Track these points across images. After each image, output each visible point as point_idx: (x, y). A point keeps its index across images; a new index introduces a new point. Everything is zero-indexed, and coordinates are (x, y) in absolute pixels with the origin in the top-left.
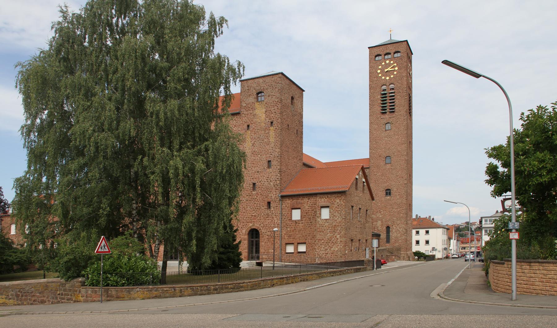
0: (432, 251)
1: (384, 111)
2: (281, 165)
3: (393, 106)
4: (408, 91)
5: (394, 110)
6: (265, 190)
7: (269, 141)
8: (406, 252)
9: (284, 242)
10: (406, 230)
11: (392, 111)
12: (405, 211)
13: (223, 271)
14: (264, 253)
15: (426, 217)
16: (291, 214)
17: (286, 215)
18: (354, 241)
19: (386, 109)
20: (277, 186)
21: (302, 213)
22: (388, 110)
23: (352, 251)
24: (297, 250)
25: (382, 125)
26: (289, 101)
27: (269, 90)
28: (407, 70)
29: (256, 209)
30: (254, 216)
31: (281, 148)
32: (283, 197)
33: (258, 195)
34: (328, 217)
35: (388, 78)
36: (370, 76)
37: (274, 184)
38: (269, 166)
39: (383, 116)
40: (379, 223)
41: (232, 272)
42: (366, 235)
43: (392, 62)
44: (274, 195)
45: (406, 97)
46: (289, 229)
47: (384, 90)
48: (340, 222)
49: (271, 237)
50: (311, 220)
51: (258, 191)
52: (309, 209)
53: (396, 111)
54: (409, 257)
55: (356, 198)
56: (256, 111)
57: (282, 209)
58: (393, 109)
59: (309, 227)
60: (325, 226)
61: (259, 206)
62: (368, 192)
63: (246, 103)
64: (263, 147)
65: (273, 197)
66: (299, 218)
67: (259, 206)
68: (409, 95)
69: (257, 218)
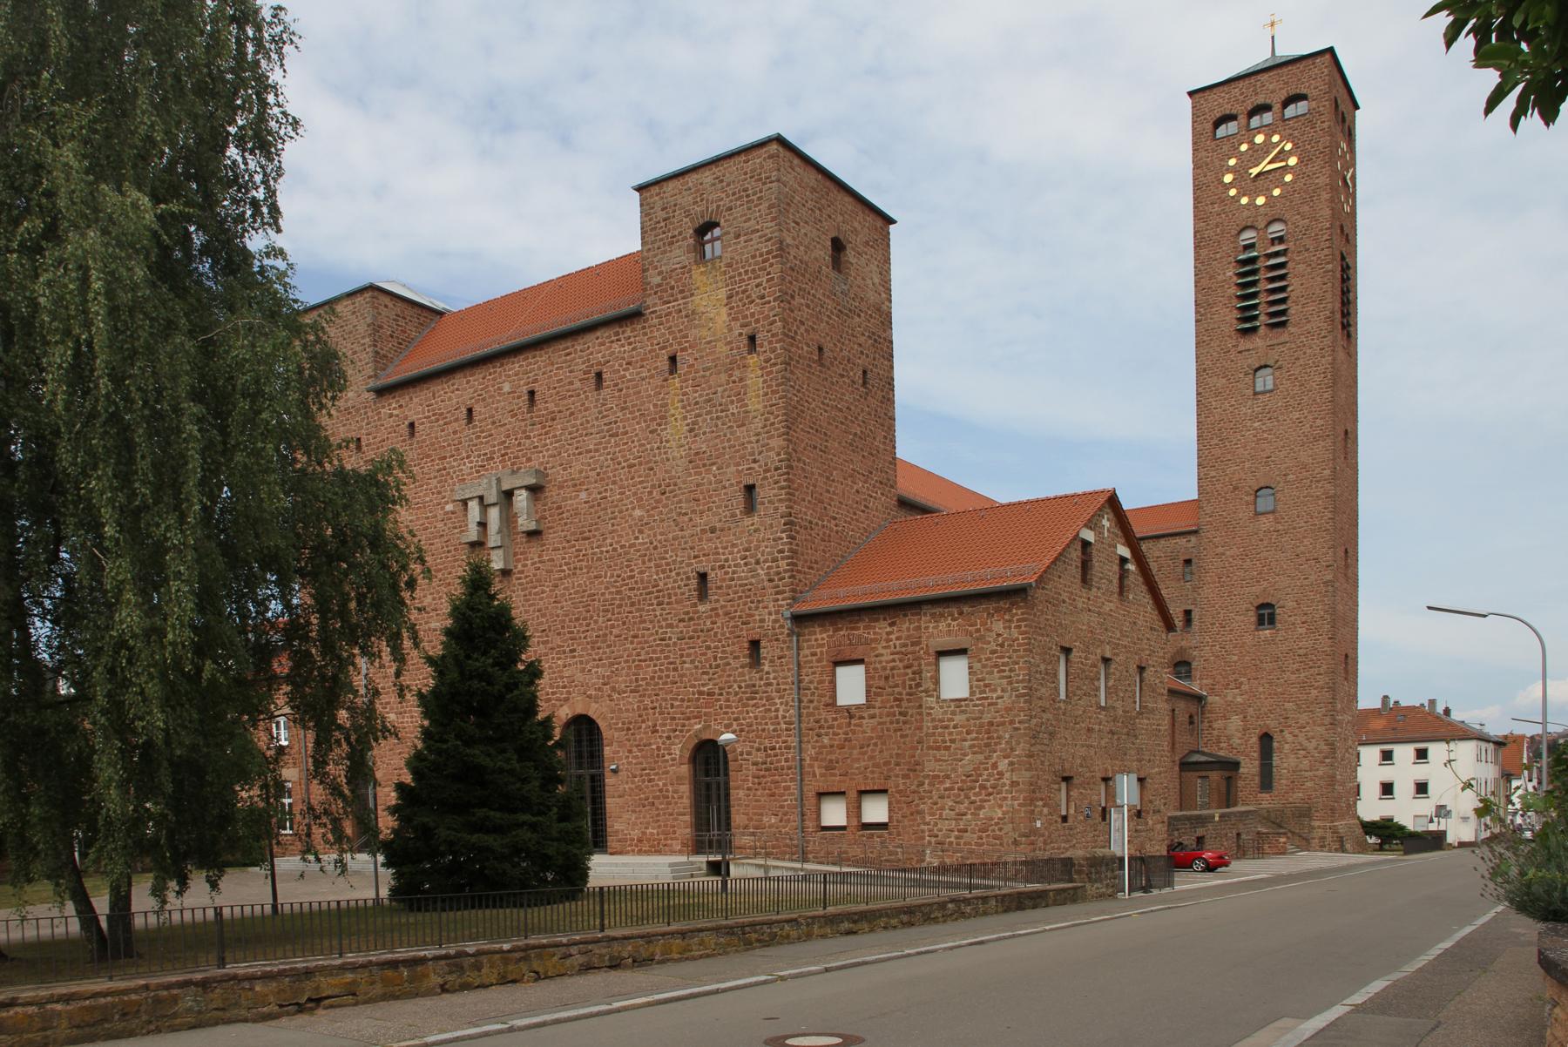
0: (1435, 819)
3: (1283, 301)
5: (1284, 319)
6: (740, 598)
10: (1331, 745)
11: (1279, 322)
13: (501, 899)
14: (746, 827)
16: (833, 683)
17: (816, 688)
18: (1075, 781)
19: (1255, 318)
20: (780, 580)
22: (1263, 318)
23: (1070, 820)
24: (859, 815)
25: (1241, 376)
26: (823, 253)
27: (737, 212)
28: (1332, 163)
30: (708, 694)
31: (788, 434)
32: (799, 619)
33: (717, 615)
35: (1260, 201)
36: (1197, 200)
37: (768, 574)
38: (750, 507)
39: (1245, 343)
40: (1235, 722)
41: (494, 902)
42: (1140, 761)
43: (1276, 138)
44: (770, 614)
46: (826, 741)
47: (1247, 247)
48: (1008, 710)
49: (766, 770)
50: (904, 704)
51: (717, 601)
52: (894, 660)
54: (1341, 840)
55: (1085, 617)
56: (696, 299)
57: (799, 665)
58: (1283, 313)
59: (895, 731)
60: (955, 727)
61: (721, 658)
62: (1147, 600)
63: (660, 273)
65: (768, 624)
66: (860, 699)
67: (721, 658)
68: (1343, 258)
69: (719, 700)
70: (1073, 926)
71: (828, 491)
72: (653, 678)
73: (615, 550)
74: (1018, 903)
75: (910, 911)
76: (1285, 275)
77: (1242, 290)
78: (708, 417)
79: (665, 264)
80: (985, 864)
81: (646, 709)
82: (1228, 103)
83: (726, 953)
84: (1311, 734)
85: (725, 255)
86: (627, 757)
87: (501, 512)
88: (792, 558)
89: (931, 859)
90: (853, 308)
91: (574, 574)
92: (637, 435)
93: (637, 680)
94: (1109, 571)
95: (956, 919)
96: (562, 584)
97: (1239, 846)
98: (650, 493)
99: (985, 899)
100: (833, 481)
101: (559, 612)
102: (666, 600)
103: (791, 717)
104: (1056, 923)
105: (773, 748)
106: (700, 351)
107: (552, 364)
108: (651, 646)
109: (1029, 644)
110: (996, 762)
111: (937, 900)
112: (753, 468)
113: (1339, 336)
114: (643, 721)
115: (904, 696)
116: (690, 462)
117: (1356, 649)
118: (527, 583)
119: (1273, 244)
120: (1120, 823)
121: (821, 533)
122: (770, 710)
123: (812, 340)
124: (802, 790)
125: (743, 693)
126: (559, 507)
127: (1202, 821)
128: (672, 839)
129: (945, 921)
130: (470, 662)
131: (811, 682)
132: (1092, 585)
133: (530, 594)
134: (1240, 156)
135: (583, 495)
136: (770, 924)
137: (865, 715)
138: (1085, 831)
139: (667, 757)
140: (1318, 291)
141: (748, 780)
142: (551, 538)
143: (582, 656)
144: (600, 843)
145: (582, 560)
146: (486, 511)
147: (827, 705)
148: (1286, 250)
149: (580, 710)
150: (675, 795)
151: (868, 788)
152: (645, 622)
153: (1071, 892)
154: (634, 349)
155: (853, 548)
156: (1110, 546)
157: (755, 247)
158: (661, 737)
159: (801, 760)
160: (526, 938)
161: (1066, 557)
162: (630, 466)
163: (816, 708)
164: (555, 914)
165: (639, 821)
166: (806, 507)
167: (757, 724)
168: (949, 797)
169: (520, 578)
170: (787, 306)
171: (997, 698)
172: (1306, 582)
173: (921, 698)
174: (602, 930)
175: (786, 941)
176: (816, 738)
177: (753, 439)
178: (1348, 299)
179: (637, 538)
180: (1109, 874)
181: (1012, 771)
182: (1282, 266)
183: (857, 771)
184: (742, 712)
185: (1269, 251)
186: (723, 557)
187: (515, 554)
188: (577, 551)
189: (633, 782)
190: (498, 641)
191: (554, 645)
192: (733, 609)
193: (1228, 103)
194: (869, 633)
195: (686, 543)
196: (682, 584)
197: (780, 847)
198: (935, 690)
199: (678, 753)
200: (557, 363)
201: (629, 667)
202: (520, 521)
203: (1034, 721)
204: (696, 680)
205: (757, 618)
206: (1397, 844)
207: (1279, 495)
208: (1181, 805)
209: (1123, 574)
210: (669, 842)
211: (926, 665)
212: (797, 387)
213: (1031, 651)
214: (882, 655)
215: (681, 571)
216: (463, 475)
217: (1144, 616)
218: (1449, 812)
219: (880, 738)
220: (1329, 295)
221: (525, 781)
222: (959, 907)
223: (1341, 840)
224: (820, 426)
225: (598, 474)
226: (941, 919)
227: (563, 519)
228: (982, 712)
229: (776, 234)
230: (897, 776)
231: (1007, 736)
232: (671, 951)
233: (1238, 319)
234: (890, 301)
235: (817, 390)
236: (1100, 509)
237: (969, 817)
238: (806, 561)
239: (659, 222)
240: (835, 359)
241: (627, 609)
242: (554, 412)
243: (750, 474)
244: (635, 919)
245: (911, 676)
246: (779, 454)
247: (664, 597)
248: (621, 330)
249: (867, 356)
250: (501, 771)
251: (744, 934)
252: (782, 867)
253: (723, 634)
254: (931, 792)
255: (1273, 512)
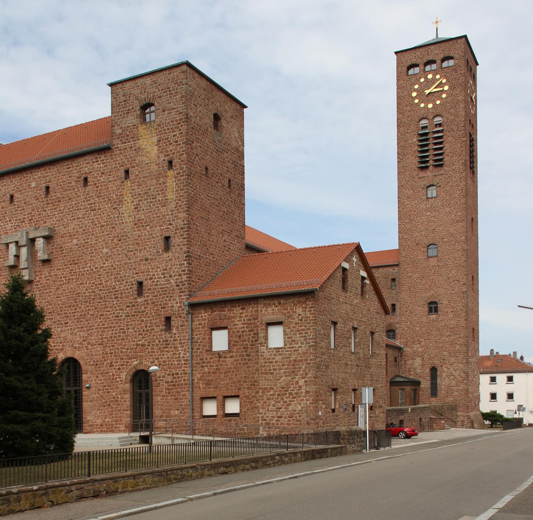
0: (518, 412)
1: (423, 165)
2: (189, 243)
3: (441, 154)
4: (468, 127)
5: (442, 163)
6: (161, 295)
7: (166, 199)
8: (468, 413)
9: (198, 395)
10: (467, 374)
12: (464, 340)
14: (161, 416)
15: (510, 354)
16: (210, 339)
17: (201, 342)
18: (339, 391)
19: (427, 162)
20: (183, 285)
21: (230, 336)
22: (431, 162)
23: (336, 411)
25: (421, 189)
26: (209, 121)
27: (164, 99)
28: (465, 90)
29: (144, 331)
30: (142, 345)
32: (193, 306)
33: (148, 304)
34: (281, 345)
35: (430, 106)
36: (398, 104)
37: (176, 282)
39: (422, 174)
40: (418, 361)
42: (372, 380)
43: (438, 77)
44: (177, 303)
45: (464, 139)
46: (206, 370)
48: (304, 353)
49: (173, 385)
50: (249, 350)
51: (148, 296)
52: (243, 327)
53: (446, 163)
54: (472, 422)
55: (344, 306)
56: (141, 142)
57: (192, 330)
58: (441, 160)
59: (244, 364)
60: (276, 362)
61: (149, 326)
62: (375, 298)
63: (121, 128)
64: (154, 211)
65: (176, 308)
67: (149, 326)
68: (470, 135)
69: (147, 349)
70: (343, 467)
71: (209, 240)
72: (111, 337)
73: (92, 270)
74: (313, 455)
75: (256, 460)
76: (443, 142)
77: (420, 148)
78: (146, 202)
79: (124, 124)
80: (293, 435)
81: (107, 354)
82: (414, 58)
83: (157, 486)
84: (456, 368)
85: (157, 120)
86: (95, 380)
87: (28, 249)
88: (190, 274)
89: (263, 433)
90: (224, 149)
91: (69, 282)
92: (106, 210)
93: (102, 338)
94: (357, 283)
95: (280, 465)
96: (61, 288)
97: (421, 425)
98: (112, 240)
99: (295, 454)
100: (212, 235)
101: (59, 302)
102: (120, 296)
103: (187, 357)
104: (334, 466)
105: (177, 374)
106: (142, 168)
107: (60, 173)
108: (111, 320)
109: (315, 320)
110: (298, 381)
111: (270, 454)
112: (170, 228)
113: (469, 172)
114: (105, 360)
115: (249, 346)
116: (135, 224)
117: (478, 325)
118: (42, 287)
119: (436, 127)
120: (363, 414)
121: (205, 262)
122: (175, 354)
123: (202, 164)
124: (192, 396)
125: (161, 345)
126: (61, 247)
127: (402, 412)
128: (120, 424)
129: (274, 466)
130: (11, 330)
131: (199, 339)
132: (347, 290)
133: (43, 293)
134: (420, 84)
135: (75, 241)
136: (182, 469)
137: (228, 356)
138: (344, 417)
139: (118, 380)
140: (458, 151)
141: (163, 391)
142: (56, 263)
143: (72, 326)
144: (79, 428)
145: (74, 275)
146: (19, 249)
147: (207, 351)
148: (443, 130)
149: (69, 355)
150: (122, 400)
151: (229, 395)
152: (108, 307)
153: (340, 449)
154: (105, 166)
155: (222, 269)
156: (357, 271)
157: (174, 116)
158: (115, 369)
159: (192, 380)
160: (46, 482)
161: (334, 276)
162: (102, 226)
163: (201, 352)
164: (56, 468)
165: (101, 415)
166: (197, 248)
167: (168, 361)
168: (272, 399)
169: (38, 285)
170: (190, 146)
171: (299, 347)
172: (453, 292)
173: (258, 347)
174: (89, 476)
175: (190, 479)
176: (200, 368)
177: (170, 213)
178: (473, 155)
179: (104, 263)
180: (359, 440)
181: (306, 385)
182: (441, 137)
183: (223, 386)
184: (160, 355)
185: (434, 130)
186: (152, 274)
187: (35, 272)
188: (70, 270)
189: (98, 393)
190: (27, 318)
191: (56, 320)
192: (156, 301)
193: (414, 58)
194: (230, 313)
195: (131, 266)
196: (129, 287)
197: (180, 427)
198: (265, 343)
199: (124, 377)
200: (62, 172)
201: (98, 332)
202: (39, 254)
203: (318, 359)
204: (135, 338)
205: (170, 305)
206: (499, 424)
207: (439, 248)
208: (391, 404)
209: (363, 285)
210: (118, 426)
211: (261, 330)
212: (194, 187)
213: (317, 324)
214: (237, 325)
215: (129, 281)
216: (7, 230)
217: (374, 307)
218: (524, 408)
219: (235, 368)
220: (464, 153)
221: (40, 394)
222: (282, 458)
223: (472, 422)
224: (205, 207)
225: (84, 230)
226: (272, 465)
227: (63, 253)
228: (290, 355)
229: (185, 111)
230: (245, 388)
231: (304, 367)
232: (128, 486)
233: (419, 162)
234: (244, 146)
235: (204, 189)
236: (352, 252)
237: (283, 409)
238: (197, 276)
239: (121, 102)
240: (214, 174)
241: (98, 301)
242: (60, 198)
243: (168, 231)
244: (101, 469)
245: (253, 335)
246: (183, 221)
247: (118, 294)
248: (98, 157)
249: (231, 173)
250: (26, 389)
251: (167, 475)
252: (182, 438)
253: (151, 314)
254: (263, 397)
255: (436, 256)
